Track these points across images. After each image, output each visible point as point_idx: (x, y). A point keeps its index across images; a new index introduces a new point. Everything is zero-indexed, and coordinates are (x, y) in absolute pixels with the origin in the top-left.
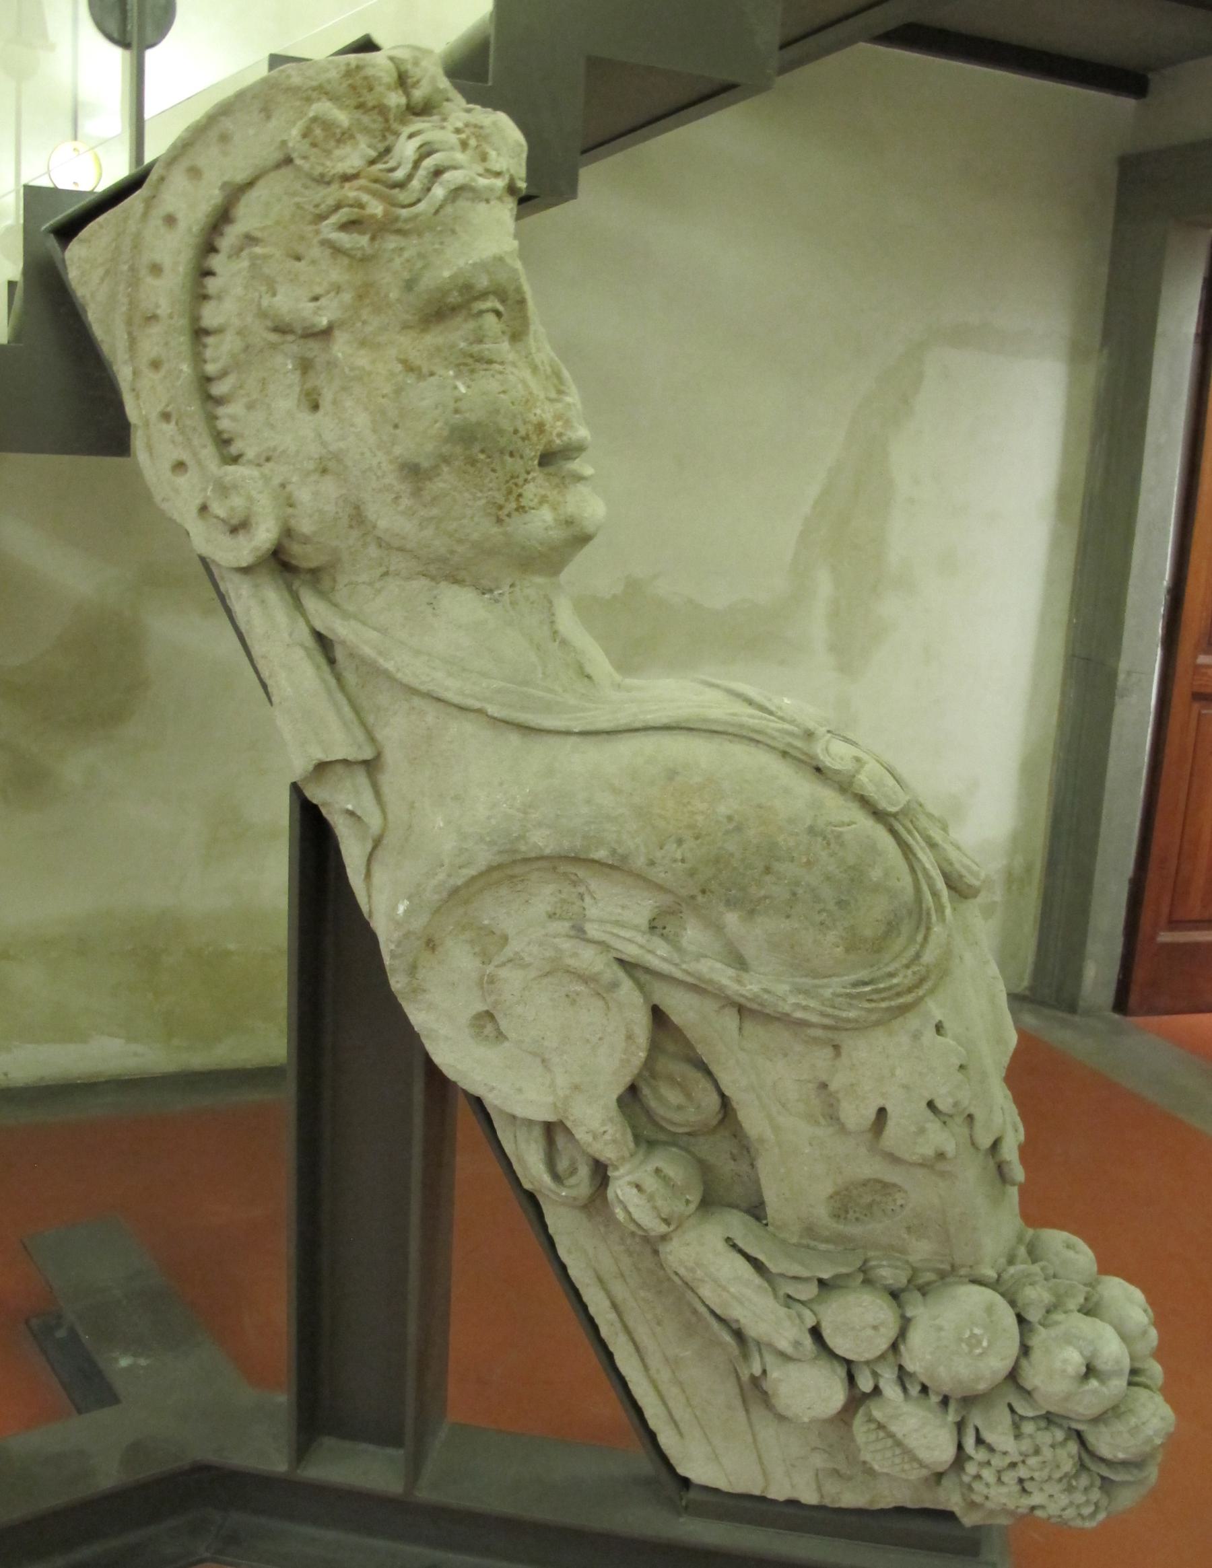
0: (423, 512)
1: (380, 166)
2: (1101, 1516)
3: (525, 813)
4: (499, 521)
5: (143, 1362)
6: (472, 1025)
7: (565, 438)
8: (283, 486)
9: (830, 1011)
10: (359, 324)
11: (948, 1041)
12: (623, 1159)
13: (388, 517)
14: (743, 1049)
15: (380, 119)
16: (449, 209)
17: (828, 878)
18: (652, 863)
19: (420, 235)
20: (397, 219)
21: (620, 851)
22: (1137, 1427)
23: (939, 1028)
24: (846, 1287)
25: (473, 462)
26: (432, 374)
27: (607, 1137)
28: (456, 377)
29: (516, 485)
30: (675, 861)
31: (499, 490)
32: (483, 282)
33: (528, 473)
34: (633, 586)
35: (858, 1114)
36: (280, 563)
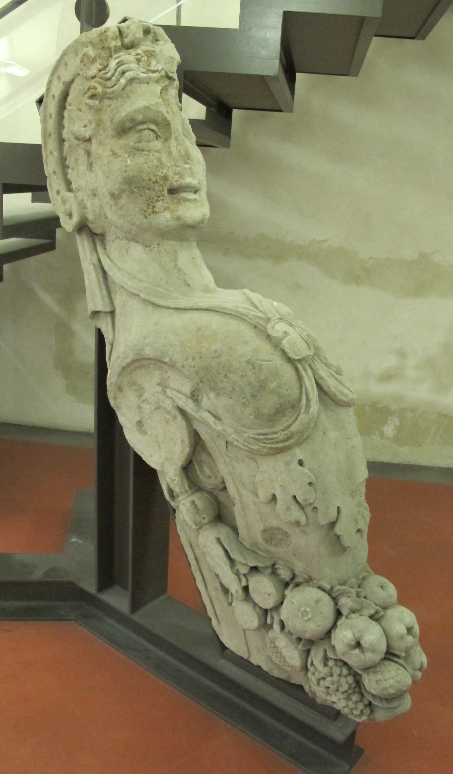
0: (119, 213)
1: (103, 72)
2: (364, 718)
3: (145, 339)
4: (146, 217)
5: (80, 541)
6: (136, 425)
7: (178, 183)
8: (82, 200)
9: (246, 444)
10: (99, 136)
11: (305, 470)
12: (182, 493)
13: (112, 215)
14: (227, 456)
15: (108, 52)
16: (129, 88)
17: (249, 384)
18: (183, 367)
19: (117, 99)
20: (106, 93)
21: (173, 360)
22: (380, 680)
23: (301, 463)
24: (262, 573)
25: (133, 192)
26: (120, 156)
27: (175, 482)
28: (128, 157)
29: (152, 202)
30: (191, 367)
31: (144, 204)
32: (140, 117)
33: (159, 197)
34: (423, 256)
35: (264, 494)
36: (83, 227)
